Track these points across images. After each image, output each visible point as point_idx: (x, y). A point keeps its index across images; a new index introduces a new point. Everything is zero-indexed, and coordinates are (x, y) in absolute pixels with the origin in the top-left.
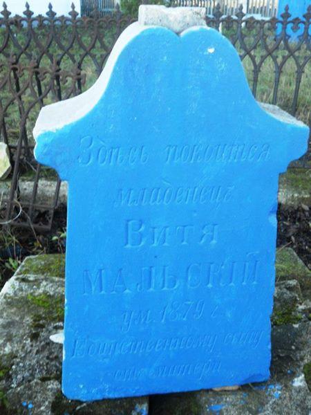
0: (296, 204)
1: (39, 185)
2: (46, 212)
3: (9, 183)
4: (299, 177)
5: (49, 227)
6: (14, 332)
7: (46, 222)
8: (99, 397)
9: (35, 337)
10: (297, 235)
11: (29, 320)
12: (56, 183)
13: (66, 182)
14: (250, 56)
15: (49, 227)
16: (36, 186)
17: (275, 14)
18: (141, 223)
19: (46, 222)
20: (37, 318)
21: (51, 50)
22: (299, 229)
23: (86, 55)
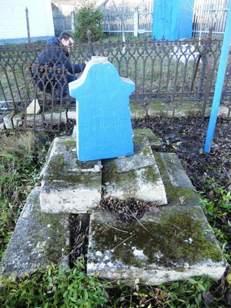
0: (155, 116)
1: (53, 116)
2: (57, 125)
3: (40, 115)
4: (156, 105)
5: (58, 131)
6: (61, 149)
7: (57, 129)
8: (88, 160)
9: (67, 150)
10: (155, 126)
11: (65, 147)
12: (59, 114)
13: (95, 62)
14: (113, 55)
15: (58, 131)
16: (52, 115)
17: (35, 102)
18: (96, 110)
19: (57, 129)
20: (67, 146)
21: (10, 63)
22: (156, 125)
23: (214, 52)
